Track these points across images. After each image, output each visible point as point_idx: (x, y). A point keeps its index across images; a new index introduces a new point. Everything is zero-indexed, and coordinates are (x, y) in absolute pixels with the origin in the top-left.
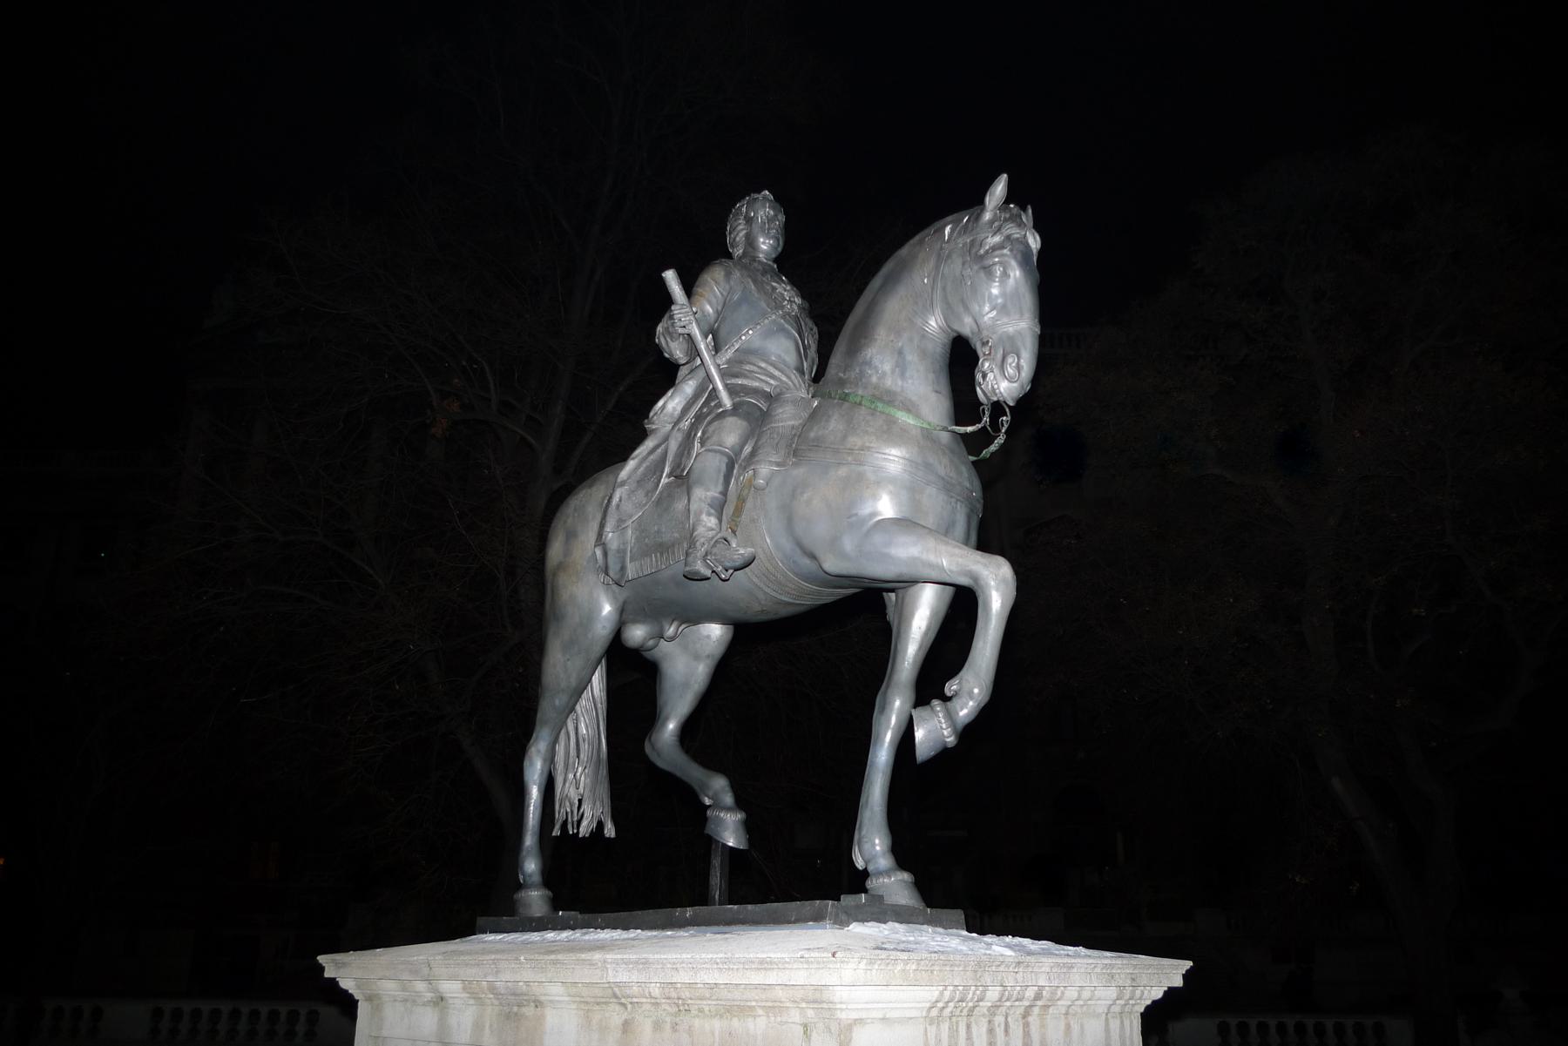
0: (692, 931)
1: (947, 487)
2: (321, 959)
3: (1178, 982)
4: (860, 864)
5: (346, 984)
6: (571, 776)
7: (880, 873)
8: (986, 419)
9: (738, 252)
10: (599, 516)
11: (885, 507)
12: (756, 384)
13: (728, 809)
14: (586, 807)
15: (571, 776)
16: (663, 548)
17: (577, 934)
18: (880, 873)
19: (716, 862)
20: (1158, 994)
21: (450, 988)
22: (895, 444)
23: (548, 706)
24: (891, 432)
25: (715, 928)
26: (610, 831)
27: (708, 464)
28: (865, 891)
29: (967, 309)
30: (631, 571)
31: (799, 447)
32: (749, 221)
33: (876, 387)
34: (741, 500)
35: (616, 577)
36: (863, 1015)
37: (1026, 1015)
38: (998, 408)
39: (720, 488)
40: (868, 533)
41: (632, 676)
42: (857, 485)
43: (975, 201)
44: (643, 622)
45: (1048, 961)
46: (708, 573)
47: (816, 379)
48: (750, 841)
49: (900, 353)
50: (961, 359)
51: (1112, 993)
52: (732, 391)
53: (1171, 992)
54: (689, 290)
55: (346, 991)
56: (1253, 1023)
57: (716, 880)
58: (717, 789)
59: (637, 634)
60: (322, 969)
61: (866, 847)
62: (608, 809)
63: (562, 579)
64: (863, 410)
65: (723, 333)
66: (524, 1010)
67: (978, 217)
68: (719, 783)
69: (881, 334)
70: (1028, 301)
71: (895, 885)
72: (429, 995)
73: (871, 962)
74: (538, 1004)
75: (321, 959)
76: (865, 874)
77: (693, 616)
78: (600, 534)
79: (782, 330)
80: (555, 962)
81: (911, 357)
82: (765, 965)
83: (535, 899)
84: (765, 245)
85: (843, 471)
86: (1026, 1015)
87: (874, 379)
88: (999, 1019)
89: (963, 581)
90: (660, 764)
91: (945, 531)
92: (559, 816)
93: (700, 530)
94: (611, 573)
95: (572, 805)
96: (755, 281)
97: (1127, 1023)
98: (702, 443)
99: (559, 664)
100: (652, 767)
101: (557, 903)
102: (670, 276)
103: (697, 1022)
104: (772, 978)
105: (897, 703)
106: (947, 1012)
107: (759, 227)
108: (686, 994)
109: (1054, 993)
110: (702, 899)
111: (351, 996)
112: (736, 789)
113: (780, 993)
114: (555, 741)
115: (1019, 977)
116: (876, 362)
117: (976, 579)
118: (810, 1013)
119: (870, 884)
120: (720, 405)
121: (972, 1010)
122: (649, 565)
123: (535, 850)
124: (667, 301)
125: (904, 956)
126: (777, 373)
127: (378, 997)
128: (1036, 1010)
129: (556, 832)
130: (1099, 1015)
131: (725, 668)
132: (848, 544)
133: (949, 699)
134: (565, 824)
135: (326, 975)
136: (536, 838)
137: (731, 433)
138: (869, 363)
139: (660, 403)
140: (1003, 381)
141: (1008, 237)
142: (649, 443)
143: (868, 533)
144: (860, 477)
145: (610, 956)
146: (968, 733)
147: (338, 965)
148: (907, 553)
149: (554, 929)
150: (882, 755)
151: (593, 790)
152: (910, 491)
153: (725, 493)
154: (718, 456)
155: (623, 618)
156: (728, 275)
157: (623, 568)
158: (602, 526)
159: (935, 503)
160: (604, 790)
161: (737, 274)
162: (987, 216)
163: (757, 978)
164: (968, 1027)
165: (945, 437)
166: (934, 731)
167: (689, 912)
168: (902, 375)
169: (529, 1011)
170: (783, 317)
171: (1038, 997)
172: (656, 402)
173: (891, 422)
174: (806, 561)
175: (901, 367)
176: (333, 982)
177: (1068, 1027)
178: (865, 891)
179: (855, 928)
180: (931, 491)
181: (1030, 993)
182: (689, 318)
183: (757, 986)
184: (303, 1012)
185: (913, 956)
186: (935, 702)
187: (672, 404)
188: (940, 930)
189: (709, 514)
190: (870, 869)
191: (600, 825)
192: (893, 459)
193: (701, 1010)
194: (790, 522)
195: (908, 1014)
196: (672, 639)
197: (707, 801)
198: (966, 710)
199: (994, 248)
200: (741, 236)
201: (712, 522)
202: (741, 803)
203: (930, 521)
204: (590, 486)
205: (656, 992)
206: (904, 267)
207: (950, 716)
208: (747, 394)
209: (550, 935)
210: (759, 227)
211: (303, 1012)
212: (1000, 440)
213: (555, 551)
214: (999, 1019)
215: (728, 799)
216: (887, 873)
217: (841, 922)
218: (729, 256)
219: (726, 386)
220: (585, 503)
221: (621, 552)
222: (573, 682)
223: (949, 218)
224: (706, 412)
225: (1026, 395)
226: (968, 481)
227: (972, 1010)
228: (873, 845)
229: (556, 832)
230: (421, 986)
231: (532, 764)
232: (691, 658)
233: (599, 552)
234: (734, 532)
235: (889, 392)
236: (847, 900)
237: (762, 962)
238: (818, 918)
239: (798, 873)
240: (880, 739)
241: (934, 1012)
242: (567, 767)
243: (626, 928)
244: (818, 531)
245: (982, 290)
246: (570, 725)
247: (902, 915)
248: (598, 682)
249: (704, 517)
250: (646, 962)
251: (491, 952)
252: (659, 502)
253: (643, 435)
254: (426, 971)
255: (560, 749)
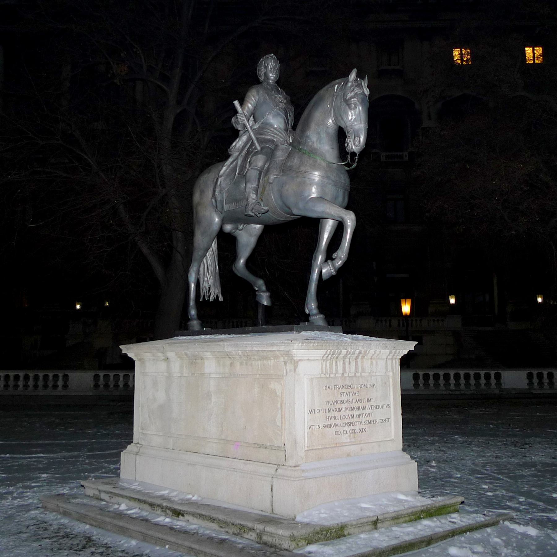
0: (252, 334)
1: (335, 184)
2: (121, 347)
3: (413, 349)
4: (307, 312)
5: (130, 355)
6: (206, 279)
7: (313, 315)
8: (349, 160)
9: (262, 79)
10: (213, 186)
11: (314, 192)
12: (269, 137)
13: (264, 292)
14: (212, 290)
15: (206, 279)
16: (237, 201)
17: (213, 336)
18: (313, 315)
19: (260, 310)
20: (406, 353)
21: (171, 355)
22: (316, 170)
23: (197, 254)
24: (315, 167)
25: (259, 334)
26: (221, 299)
27: (253, 174)
28: (308, 321)
29: (342, 119)
30: (226, 208)
31: (285, 169)
32: (266, 67)
33: (311, 147)
34: (264, 188)
35: (221, 210)
36: (302, 359)
37: (356, 358)
38: (353, 154)
39: (257, 183)
40: (307, 202)
41: (227, 243)
42: (304, 185)
43: (346, 75)
44: (231, 224)
45: (362, 343)
46: (253, 214)
47: (294, 128)
48: (273, 303)
49: (319, 133)
50: (341, 135)
51: (387, 352)
52: (260, 141)
53: (410, 352)
54: (241, 104)
55: (130, 358)
56: (545, 373)
57: (260, 316)
58: (260, 284)
59: (228, 228)
60: (121, 350)
61: (309, 306)
62: (220, 290)
63: (200, 208)
64: (306, 156)
65: (256, 115)
66: (197, 361)
67: (346, 83)
68: (261, 282)
69: (313, 126)
70: (364, 117)
71: (318, 319)
72: (163, 358)
73: (303, 343)
74: (202, 359)
75: (121, 347)
76: (309, 315)
77: (248, 220)
78: (214, 194)
79: (279, 114)
80: (208, 346)
81: (323, 135)
82: (272, 345)
83: (195, 324)
84: (272, 76)
85: (299, 180)
86: (356, 358)
87: (310, 144)
88: (347, 360)
89: (340, 219)
90: (239, 275)
91: (333, 201)
92: (202, 295)
93: (250, 199)
94: (218, 209)
95: (206, 289)
96: (268, 95)
97: (394, 361)
98: (250, 164)
99: (200, 240)
100: (235, 275)
101: (202, 325)
102: (236, 103)
103: (253, 362)
104: (274, 348)
105: (320, 257)
106: (329, 357)
107: (269, 68)
108: (250, 354)
109: (365, 352)
110: (255, 324)
111: (132, 359)
112: (266, 284)
113: (277, 353)
114: (200, 266)
115: (352, 347)
116: (311, 137)
117: (343, 219)
118: (286, 358)
119: (310, 318)
120: (256, 148)
121: (337, 357)
122: (232, 207)
123: (194, 306)
124: (236, 112)
125: (313, 341)
126: (277, 132)
127: (143, 359)
128: (360, 357)
129: (201, 300)
130: (383, 359)
131: (261, 239)
132: (301, 205)
133: (334, 259)
134: (204, 296)
135: (123, 352)
136: (194, 302)
137: (260, 161)
138: (308, 137)
139: (234, 144)
140: (356, 143)
141: (356, 94)
142: (230, 160)
143: (307, 202)
144: (304, 182)
145: (225, 343)
146: (340, 271)
147: (127, 349)
148: (318, 210)
149: (204, 335)
150: (315, 275)
151: (214, 285)
152: (322, 186)
153: (258, 185)
154: (256, 171)
155: (223, 222)
156: (258, 92)
157: (223, 207)
158: (214, 191)
159: (331, 190)
160: (218, 284)
161: (261, 92)
162: (350, 84)
163: (270, 349)
164: (336, 362)
165: (335, 166)
166: (328, 270)
167: (250, 329)
168: (320, 142)
169: (199, 361)
170: (279, 110)
171: (360, 353)
172: (232, 143)
173: (315, 161)
174: (287, 209)
175: (319, 139)
176: (126, 355)
177: (372, 363)
178: (308, 321)
179: (303, 333)
180: (329, 186)
181: (357, 352)
182: (243, 112)
183: (270, 351)
184: (61, 375)
185: (316, 341)
186: (329, 261)
187: (239, 143)
188: (333, 333)
189: (253, 194)
190: (311, 313)
191: (217, 297)
192: (316, 176)
193: (254, 359)
194: (281, 196)
195: (317, 358)
196: (241, 230)
197: (256, 289)
198: (339, 263)
199: (351, 98)
200: (263, 69)
201: (254, 196)
202: (268, 289)
203: (328, 197)
204: (209, 173)
205: (240, 353)
206: (321, 99)
207: (333, 265)
208: (266, 143)
209: (203, 337)
210: (269, 68)
211: (61, 375)
212: (355, 165)
213: (196, 197)
214: (347, 360)
215: (264, 288)
216: (316, 315)
217: (299, 331)
218: (258, 82)
219: (257, 139)
220: (207, 179)
221: (222, 202)
222: (206, 245)
223: (337, 81)
224: (250, 152)
225: (363, 149)
226: (344, 180)
227: (337, 357)
228: (312, 306)
229: (201, 300)
230: (160, 354)
231: (191, 275)
232: (248, 237)
233: (213, 200)
234: (262, 200)
235: (315, 149)
236: (302, 324)
237: (272, 344)
238: (291, 330)
239: (286, 316)
240: (347, 233)
241: (325, 358)
242: (205, 275)
243: (229, 334)
244: (291, 200)
245: (347, 111)
246: (205, 260)
247: (320, 329)
248: (214, 245)
249: (251, 194)
250: (237, 345)
251: (186, 343)
252: (235, 183)
253: (227, 157)
254: (162, 349)
255: (201, 269)
